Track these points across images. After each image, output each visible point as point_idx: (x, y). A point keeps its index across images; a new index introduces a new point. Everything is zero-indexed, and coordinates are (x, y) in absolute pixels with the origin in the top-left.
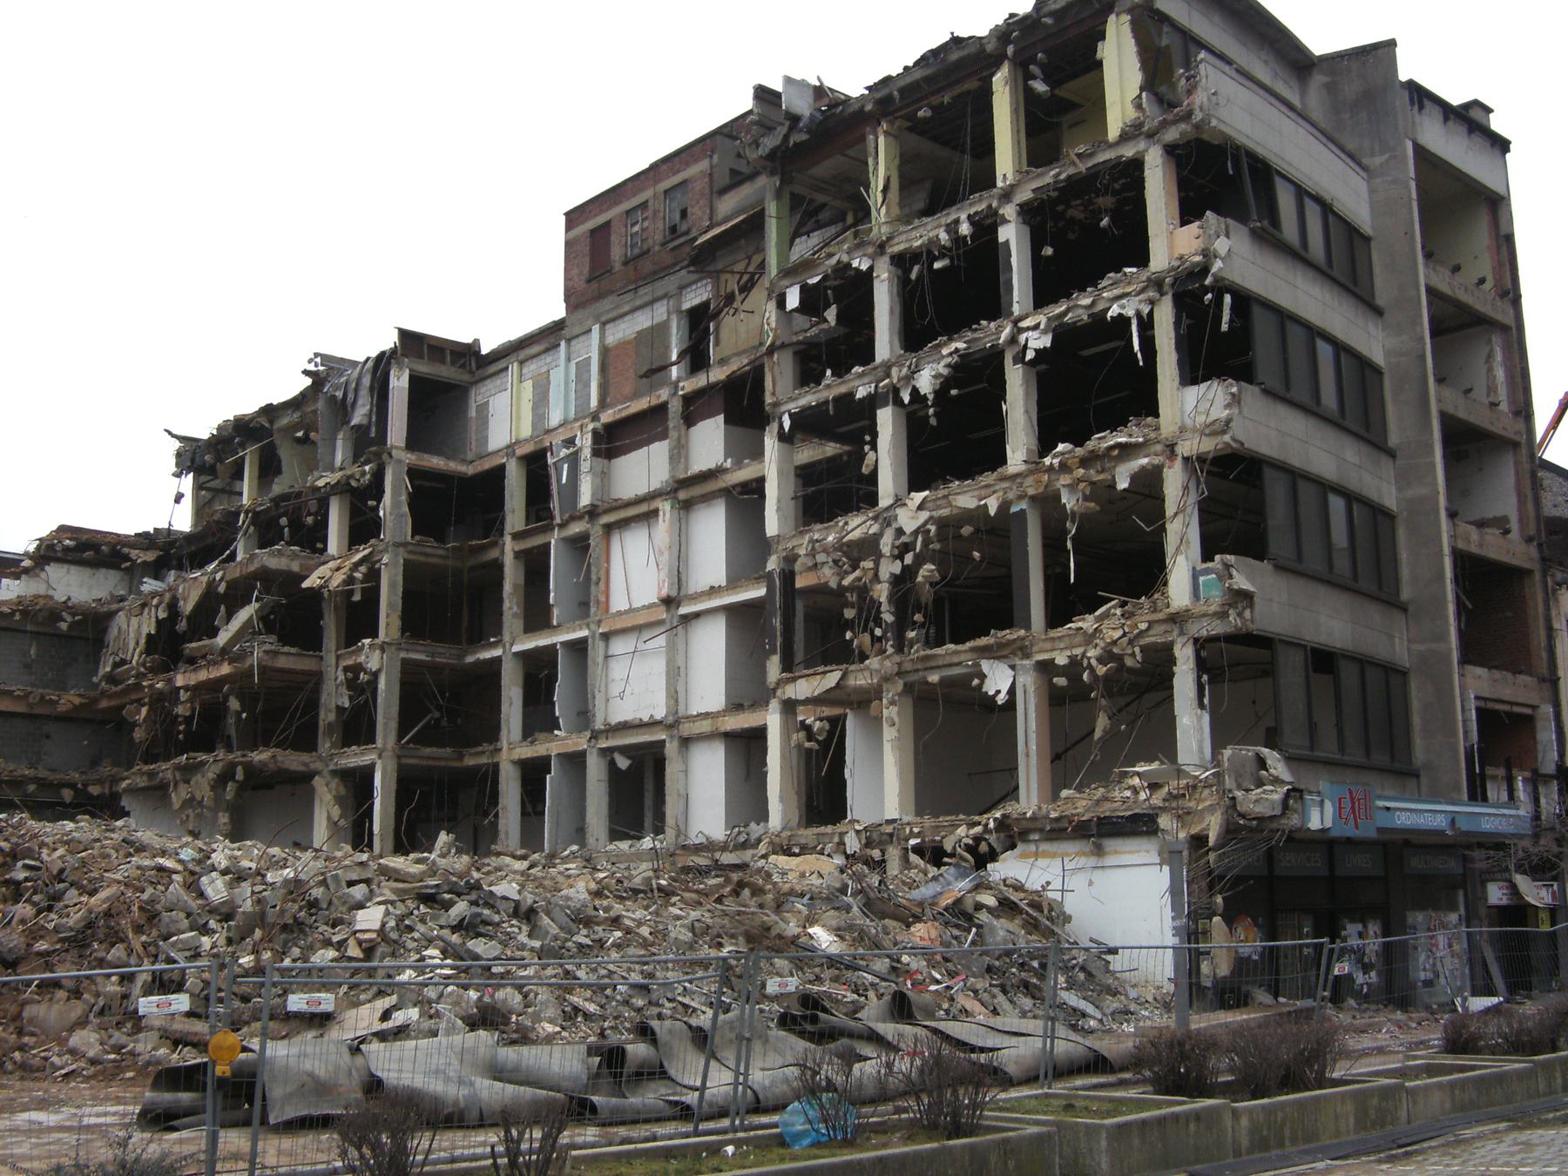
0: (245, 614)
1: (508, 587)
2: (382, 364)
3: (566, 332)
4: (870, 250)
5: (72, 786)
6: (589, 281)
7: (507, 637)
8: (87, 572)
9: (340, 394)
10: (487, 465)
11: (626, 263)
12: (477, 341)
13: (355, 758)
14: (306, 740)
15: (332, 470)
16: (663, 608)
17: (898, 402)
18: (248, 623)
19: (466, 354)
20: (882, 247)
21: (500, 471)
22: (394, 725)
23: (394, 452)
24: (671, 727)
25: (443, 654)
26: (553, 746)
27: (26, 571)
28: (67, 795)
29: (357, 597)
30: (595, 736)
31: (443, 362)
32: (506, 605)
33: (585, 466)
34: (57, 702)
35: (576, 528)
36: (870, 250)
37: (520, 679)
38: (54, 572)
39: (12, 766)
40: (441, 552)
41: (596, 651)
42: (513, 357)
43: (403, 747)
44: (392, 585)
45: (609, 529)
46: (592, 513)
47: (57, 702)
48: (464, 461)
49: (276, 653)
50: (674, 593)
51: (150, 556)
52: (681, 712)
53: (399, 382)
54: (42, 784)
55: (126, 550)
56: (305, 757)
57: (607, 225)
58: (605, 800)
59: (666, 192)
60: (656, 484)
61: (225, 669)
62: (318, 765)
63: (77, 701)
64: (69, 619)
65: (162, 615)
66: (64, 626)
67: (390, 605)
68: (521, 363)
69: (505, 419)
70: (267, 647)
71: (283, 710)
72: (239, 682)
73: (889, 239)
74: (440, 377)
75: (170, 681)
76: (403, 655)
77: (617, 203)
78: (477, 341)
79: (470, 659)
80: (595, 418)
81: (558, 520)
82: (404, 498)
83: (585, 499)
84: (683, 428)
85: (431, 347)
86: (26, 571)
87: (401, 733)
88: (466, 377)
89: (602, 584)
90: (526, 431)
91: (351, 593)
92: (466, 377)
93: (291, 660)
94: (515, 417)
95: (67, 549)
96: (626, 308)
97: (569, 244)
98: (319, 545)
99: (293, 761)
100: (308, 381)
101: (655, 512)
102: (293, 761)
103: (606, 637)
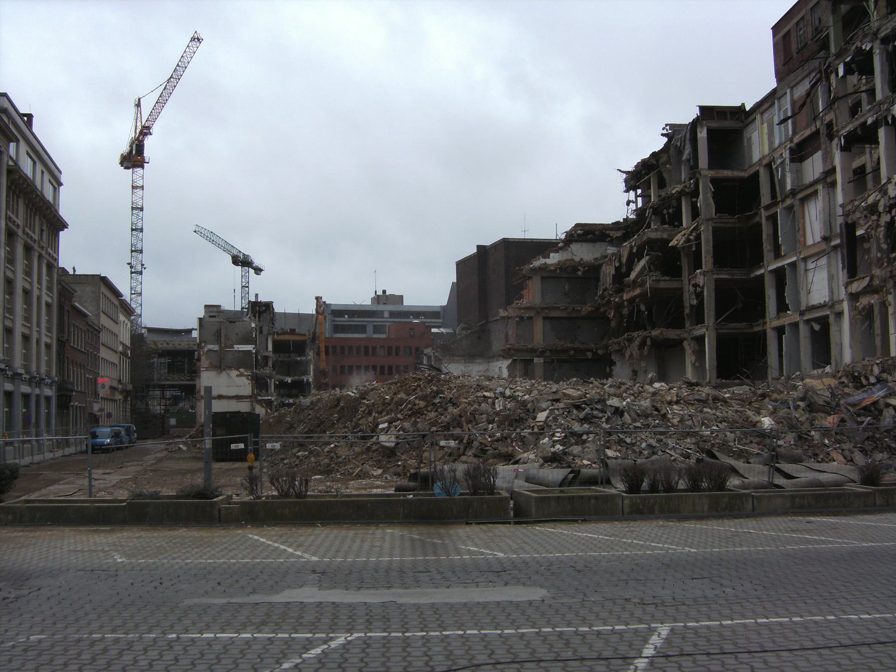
0: (643, 262)
1: (764, 237)
2: (695, 124)
3: (779, 94)
4: (869, 38)
5: (591, 350)
6: (784, 65)
7: (765, 263)
8: (591, 245)
9: (679, 144)
10: (752, 171)
11: (798, 53)
12: (743, 104)
13: (699, 331)
14: (679, 324)
15: (680, 182)
16: (824, 243)
17: (887, 124)
18: (644, 268)
19: (738, 112)
20: (875, 34)
21: (757, 174)
22: (713, 313)
23: (702, 172)
24: (832, 307)
25: (738, 274)
26: (791, 316)
27: (561, 248)
28: (589, 355)
29: (694, 249)
30: (802, 313)
31: (726, 119)
32: (764, 246)
33: (787, 168)
34: (580, 311)
35: (788, 202)
36: (869, 38)
37: (774, 284)
38: (575, 247)
39: (562, 343)
40: (731, 221)
41: (801, 266)
42: (757, 112)
43: (718, 324)
44: (707, 241)
45: (803, 201)
46: (793, 193)
47: (580, 311)
48: (743, 170)
49: (658, 281)
50: (828, 234)
51: (619, 234)
52: (836, 298)
53: (702, 134)
54: (576, 350)
55: (607, 232)
56: (678, 332)
57: (789, 31)
58: (809, 347)
59: (812, 9)
60: (817, 176)
61: (638, 291)
62: (686, 335)
63: (590, 309)
64: (582, 269)
65: (617, 265)
66: (580, 273)
67: (707, 252)
68: (762, 114)
69: (761, 143)
70: (654, 278)
71: (667, 309)
72: (643, 295)
73: (878, 30)
74: (722, 128)
75: (621, 297)
76: (716, 276)
77: (792, 19)
78: (743, 104)
79: (752, 275)
80: (792, 141)
81: (779, 199)
82: (710, 195)
83: (789, 187)
84: (828, 142)
85: (717, 112)
86: (561, 248)
87: (717, 316)
88: (740, 125)
89: (801, 232)
90: (766, 151)
91: (691, 246)
92: (740, 125)
93: (666, 283)
94: (761, 144)
95: (579, 235)
96: (800, 78)
97: (775, 45)
98: (676, 223)
99: (672, 334)
100: (665, 140)
101: (816, 193)
102: (672, 334)
103: (805, 259)
